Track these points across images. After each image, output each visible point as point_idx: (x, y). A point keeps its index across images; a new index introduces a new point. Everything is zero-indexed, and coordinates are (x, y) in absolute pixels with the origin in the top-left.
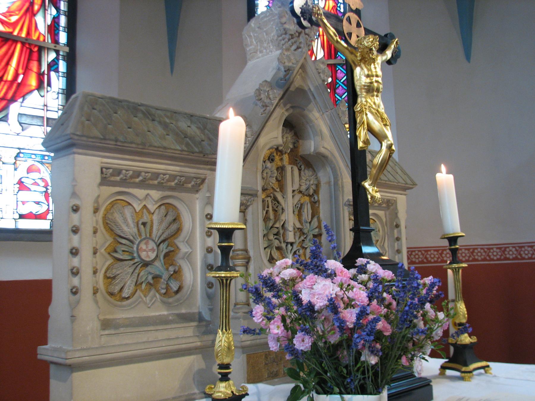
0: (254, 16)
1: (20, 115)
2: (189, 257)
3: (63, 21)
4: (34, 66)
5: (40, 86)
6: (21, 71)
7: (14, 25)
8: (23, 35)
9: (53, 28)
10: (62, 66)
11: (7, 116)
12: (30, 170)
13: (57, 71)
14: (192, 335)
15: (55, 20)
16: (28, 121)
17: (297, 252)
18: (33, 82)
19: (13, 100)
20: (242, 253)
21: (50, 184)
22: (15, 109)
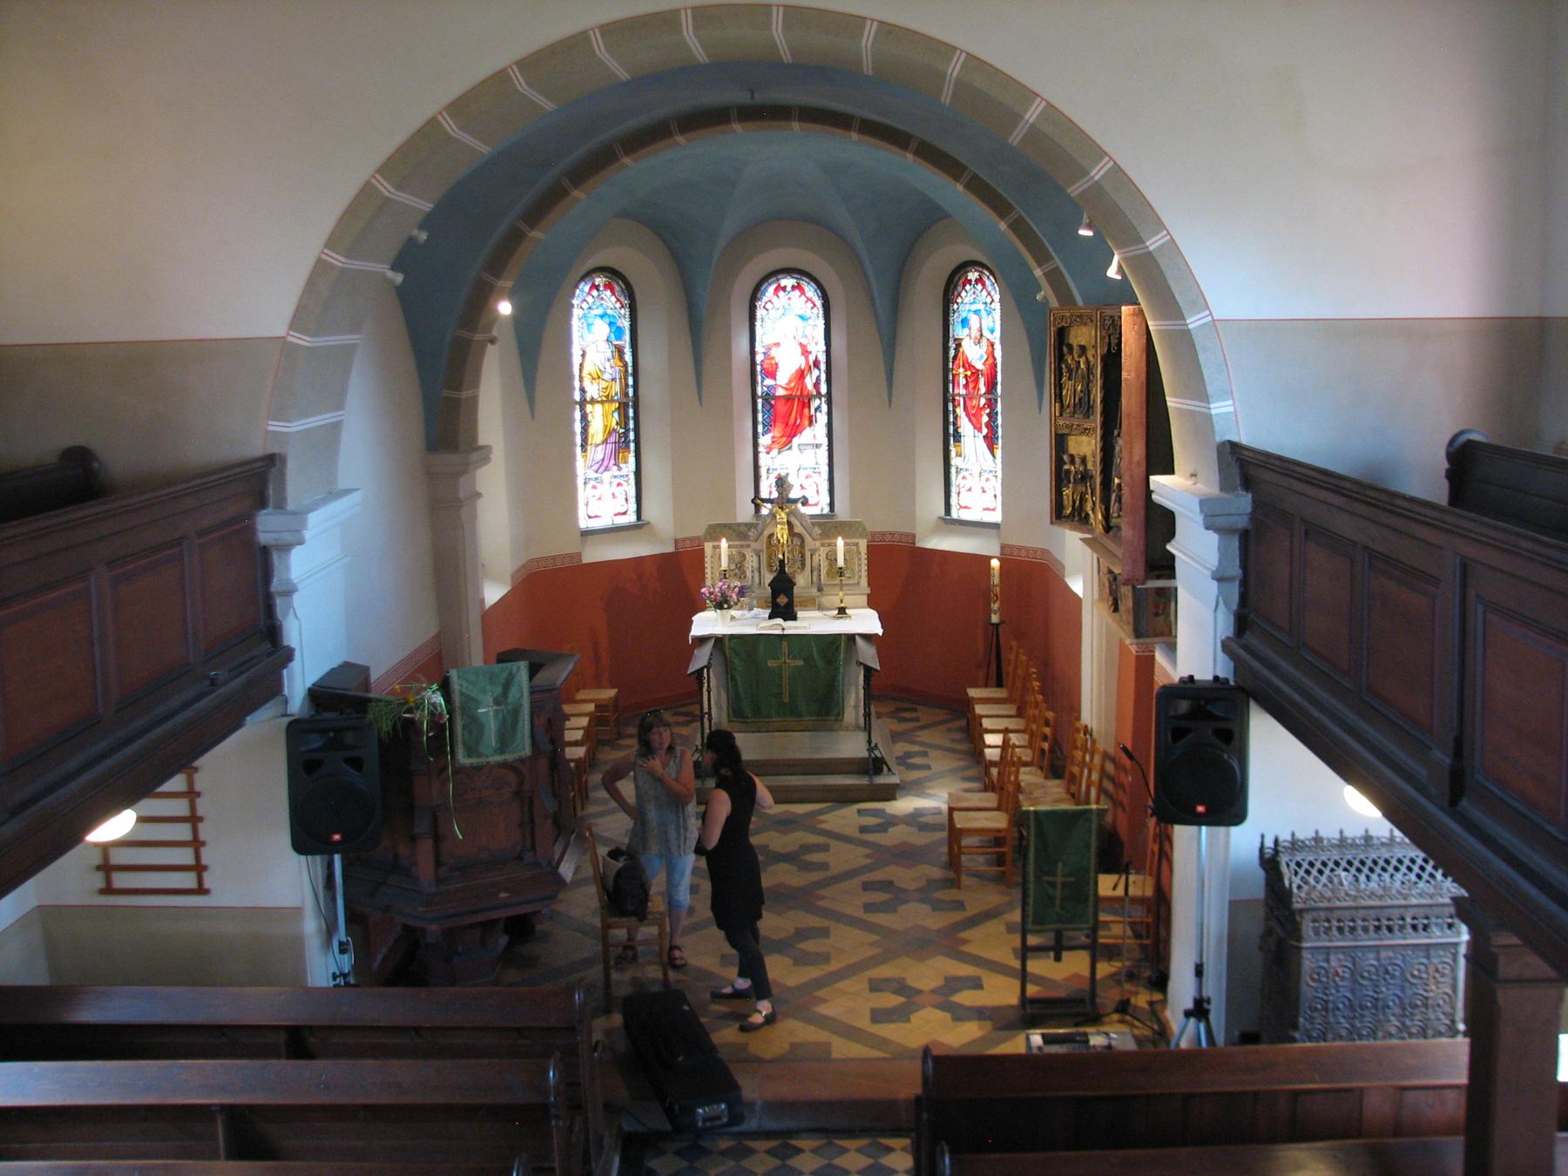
0: (1080, 599)
1: (799, 445)
2: (748, 568)
3: (823, 377)
4: (806, 411)
5: (811, 424)
6: (798, 417)
7: (792, 389)
8: (799, 393)
9: (817, 385)
10: (825, 408)
11: (791, 447)
12: (807, 477)
13: (821, 411)
14: (699, 723)
15: (818, 378)
16: (805, 447)
17: (1324, 1013)
18: (806, 422)
19: (794, 436)
20: (441, 715)
21: (578, 449)
22: (796, 441)
